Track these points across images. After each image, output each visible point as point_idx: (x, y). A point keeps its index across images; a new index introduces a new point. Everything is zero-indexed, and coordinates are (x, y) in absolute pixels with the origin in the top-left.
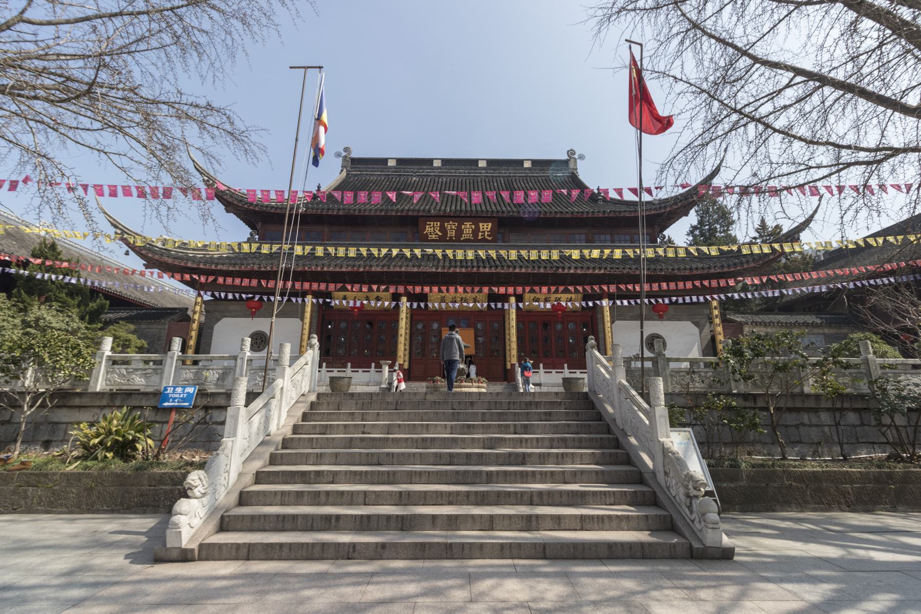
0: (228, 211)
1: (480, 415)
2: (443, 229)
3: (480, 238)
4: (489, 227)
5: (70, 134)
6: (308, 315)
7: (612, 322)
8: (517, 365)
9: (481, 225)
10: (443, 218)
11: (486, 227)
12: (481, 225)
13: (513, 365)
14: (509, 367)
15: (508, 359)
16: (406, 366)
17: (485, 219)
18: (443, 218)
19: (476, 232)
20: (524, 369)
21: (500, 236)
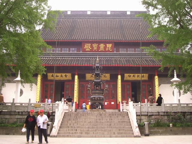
0: (162, 98)
1: (125, 136)
2: (92, 46)
3: (107, 50)
4: (111, 46)
5: (52, 33)
6: (54, 90)
7: (159, 85)
8: (121, 102)
9: (107, 45)
10: (92, 42)
11: (109, 46)
12: (107, 45)
13: (119, 102)
14: (118, 103)
15: (118, 100)
16: (77, 103)
17: (109, 43)
18: (92, 42)
19: (105, 47)
20: (122, 103)
21: (115, 49)
